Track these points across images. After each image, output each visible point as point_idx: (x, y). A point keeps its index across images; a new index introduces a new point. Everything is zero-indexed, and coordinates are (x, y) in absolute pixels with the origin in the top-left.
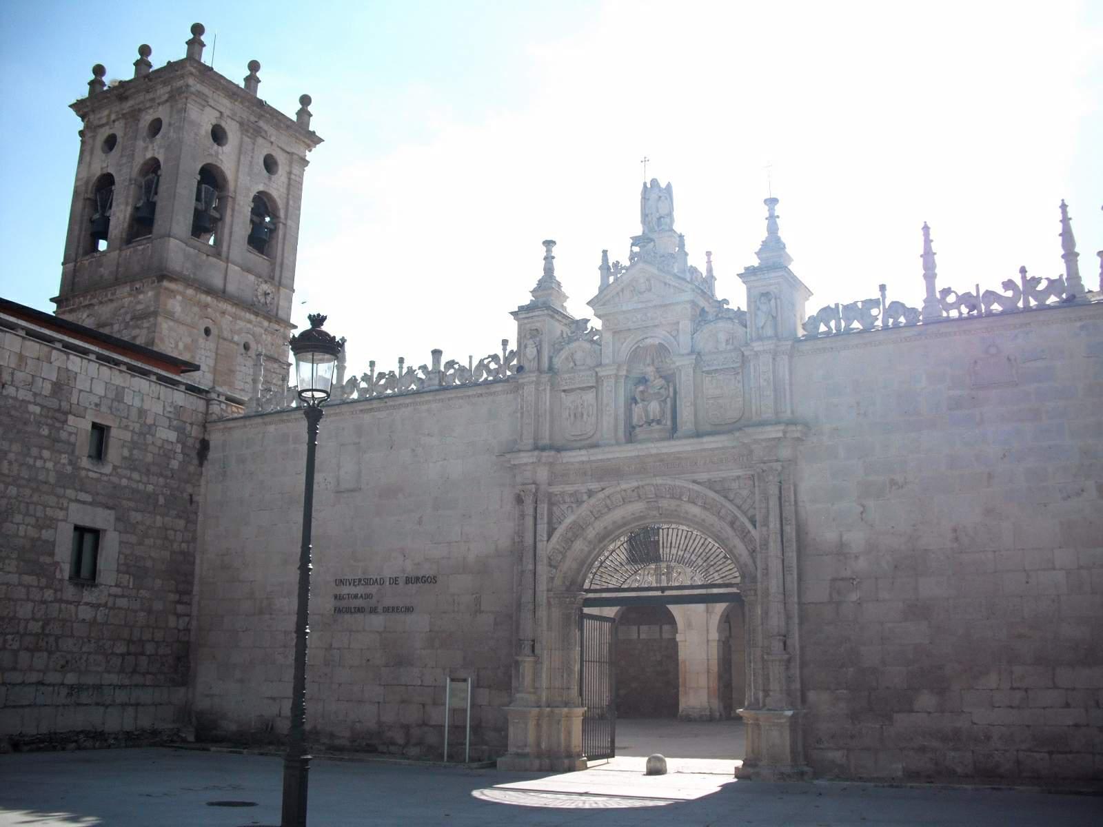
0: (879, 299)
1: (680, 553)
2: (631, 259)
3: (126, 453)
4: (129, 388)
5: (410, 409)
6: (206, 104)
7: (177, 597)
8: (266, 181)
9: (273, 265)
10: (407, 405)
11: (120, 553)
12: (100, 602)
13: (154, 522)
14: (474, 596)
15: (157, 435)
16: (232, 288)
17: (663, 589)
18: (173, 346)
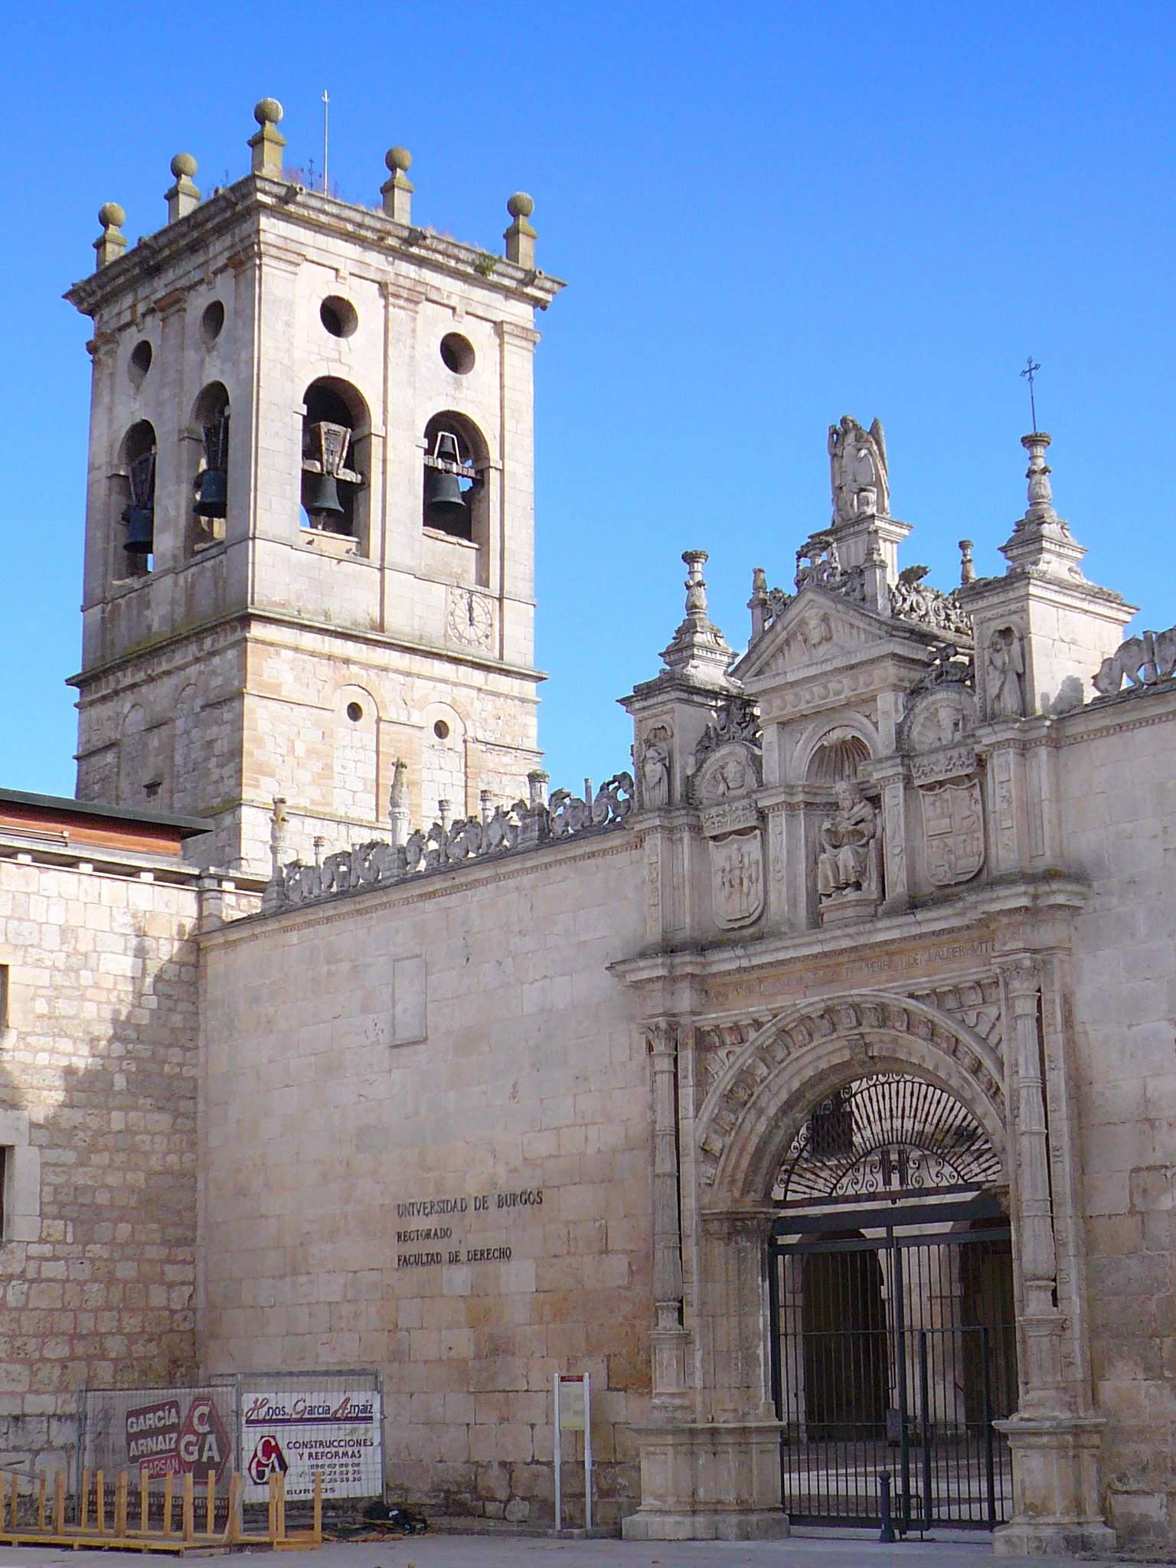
1: (918, 1127)
2: (798, 583)
3: (41, 1007)
4: (38, 893)
5: (491, 886)
6: (298, 259)
7: (164, 1252)
8: (450, 390)
9: (483, 554)
11: (42, 1183)
12: (9, 1271)
13: (109, 1122)
14: (597, 1224)
15: (102, 969)
16: (399, 623)
17: (893, 1197)
18: (283, 751)
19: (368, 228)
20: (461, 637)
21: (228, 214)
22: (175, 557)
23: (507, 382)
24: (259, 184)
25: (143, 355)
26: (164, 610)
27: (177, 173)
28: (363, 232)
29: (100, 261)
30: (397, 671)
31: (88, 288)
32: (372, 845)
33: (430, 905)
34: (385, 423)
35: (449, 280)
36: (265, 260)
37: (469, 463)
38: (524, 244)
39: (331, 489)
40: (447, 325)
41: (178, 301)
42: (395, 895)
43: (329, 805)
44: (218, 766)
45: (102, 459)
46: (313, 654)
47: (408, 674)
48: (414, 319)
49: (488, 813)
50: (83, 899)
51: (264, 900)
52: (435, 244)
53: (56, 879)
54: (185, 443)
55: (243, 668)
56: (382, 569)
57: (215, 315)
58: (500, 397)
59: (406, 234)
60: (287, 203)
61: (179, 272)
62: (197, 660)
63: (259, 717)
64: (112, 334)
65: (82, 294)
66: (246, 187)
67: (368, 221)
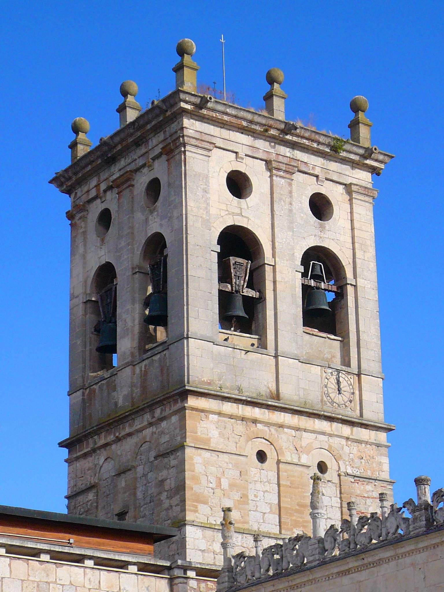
0: (128, 569)
4: (55, 582)
5: (393, 564)
8: (317, 232)
10: (388, 560)
16: (289, 393)
18: (213, 485)
19: (257, 123)
20: (333, 402)
21: (161, 118)
22: (132, 354)
23: (356, 225)
24: (182, 96)
25: (105, 218)
26: (125, 391)
27: (125, 93)
28: (253, 127)
29: (74, 155)
30: (290, 427)
31: (66, 175)
32: (298, 539)
33: (345, 580)
34: (274, 256)
35: (313, 157)
36: (188, 148)
37: (332, 282)
38: (364, 132)
39: (239, 303)
40: (312, 187)
41: (128, 180)
42: (318, 574)
43: (244, 523)
44: (167, 498)
45: (79, 290)
46: (231, 417)
47: (298, 429)
48: (290, 185)
49: (385, 509)
50: (88, 586)
51: (218, 583)
52: (303, 132)
53: (68, 572)
54: (137, 276)
55: (183, 427)
56: (276, 357)
57: (154, 187)
58: (352, 234)
59: (282, 126)
60: (201, 108)
61: (129, 160)
62: (151, 424)
63: (195, 461)
64: (84, 205)
65: (63, 180)
66: (173, 98)
67: (257, 119)
